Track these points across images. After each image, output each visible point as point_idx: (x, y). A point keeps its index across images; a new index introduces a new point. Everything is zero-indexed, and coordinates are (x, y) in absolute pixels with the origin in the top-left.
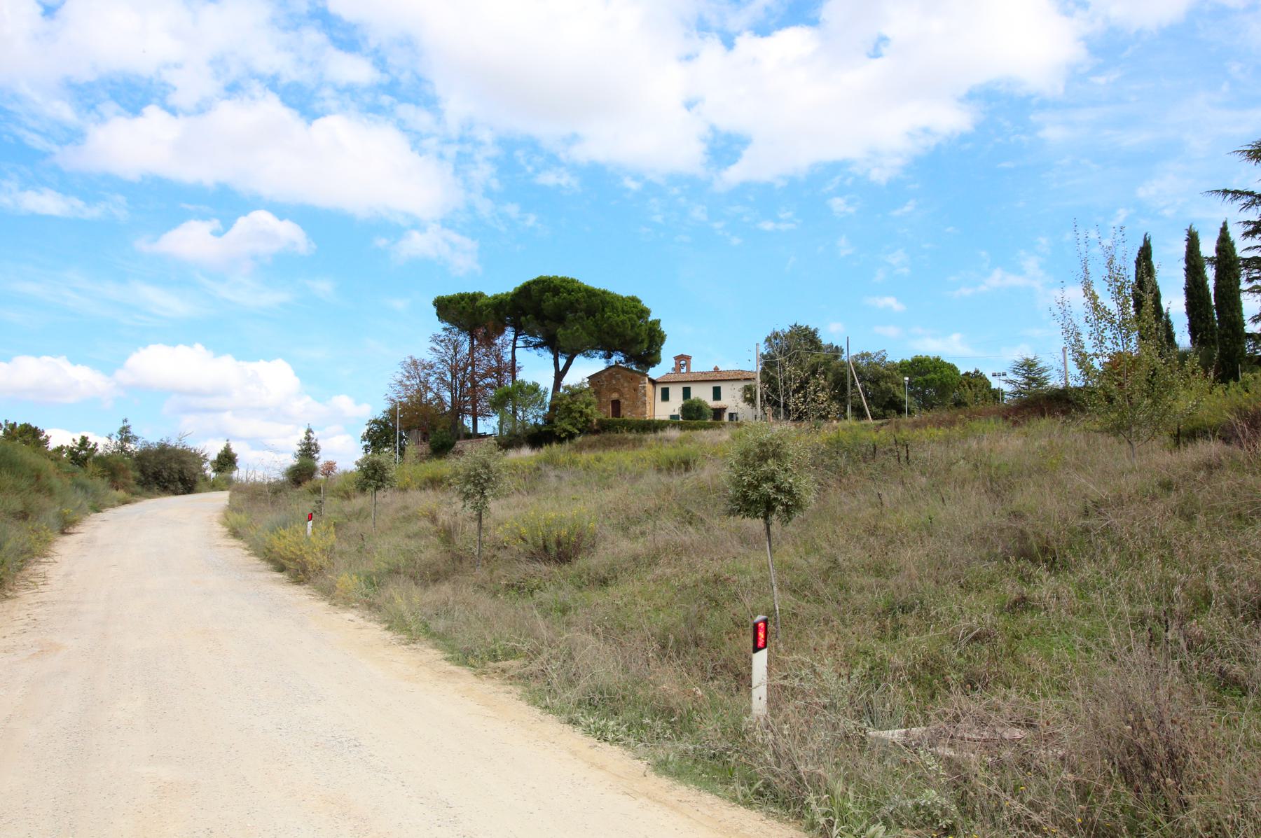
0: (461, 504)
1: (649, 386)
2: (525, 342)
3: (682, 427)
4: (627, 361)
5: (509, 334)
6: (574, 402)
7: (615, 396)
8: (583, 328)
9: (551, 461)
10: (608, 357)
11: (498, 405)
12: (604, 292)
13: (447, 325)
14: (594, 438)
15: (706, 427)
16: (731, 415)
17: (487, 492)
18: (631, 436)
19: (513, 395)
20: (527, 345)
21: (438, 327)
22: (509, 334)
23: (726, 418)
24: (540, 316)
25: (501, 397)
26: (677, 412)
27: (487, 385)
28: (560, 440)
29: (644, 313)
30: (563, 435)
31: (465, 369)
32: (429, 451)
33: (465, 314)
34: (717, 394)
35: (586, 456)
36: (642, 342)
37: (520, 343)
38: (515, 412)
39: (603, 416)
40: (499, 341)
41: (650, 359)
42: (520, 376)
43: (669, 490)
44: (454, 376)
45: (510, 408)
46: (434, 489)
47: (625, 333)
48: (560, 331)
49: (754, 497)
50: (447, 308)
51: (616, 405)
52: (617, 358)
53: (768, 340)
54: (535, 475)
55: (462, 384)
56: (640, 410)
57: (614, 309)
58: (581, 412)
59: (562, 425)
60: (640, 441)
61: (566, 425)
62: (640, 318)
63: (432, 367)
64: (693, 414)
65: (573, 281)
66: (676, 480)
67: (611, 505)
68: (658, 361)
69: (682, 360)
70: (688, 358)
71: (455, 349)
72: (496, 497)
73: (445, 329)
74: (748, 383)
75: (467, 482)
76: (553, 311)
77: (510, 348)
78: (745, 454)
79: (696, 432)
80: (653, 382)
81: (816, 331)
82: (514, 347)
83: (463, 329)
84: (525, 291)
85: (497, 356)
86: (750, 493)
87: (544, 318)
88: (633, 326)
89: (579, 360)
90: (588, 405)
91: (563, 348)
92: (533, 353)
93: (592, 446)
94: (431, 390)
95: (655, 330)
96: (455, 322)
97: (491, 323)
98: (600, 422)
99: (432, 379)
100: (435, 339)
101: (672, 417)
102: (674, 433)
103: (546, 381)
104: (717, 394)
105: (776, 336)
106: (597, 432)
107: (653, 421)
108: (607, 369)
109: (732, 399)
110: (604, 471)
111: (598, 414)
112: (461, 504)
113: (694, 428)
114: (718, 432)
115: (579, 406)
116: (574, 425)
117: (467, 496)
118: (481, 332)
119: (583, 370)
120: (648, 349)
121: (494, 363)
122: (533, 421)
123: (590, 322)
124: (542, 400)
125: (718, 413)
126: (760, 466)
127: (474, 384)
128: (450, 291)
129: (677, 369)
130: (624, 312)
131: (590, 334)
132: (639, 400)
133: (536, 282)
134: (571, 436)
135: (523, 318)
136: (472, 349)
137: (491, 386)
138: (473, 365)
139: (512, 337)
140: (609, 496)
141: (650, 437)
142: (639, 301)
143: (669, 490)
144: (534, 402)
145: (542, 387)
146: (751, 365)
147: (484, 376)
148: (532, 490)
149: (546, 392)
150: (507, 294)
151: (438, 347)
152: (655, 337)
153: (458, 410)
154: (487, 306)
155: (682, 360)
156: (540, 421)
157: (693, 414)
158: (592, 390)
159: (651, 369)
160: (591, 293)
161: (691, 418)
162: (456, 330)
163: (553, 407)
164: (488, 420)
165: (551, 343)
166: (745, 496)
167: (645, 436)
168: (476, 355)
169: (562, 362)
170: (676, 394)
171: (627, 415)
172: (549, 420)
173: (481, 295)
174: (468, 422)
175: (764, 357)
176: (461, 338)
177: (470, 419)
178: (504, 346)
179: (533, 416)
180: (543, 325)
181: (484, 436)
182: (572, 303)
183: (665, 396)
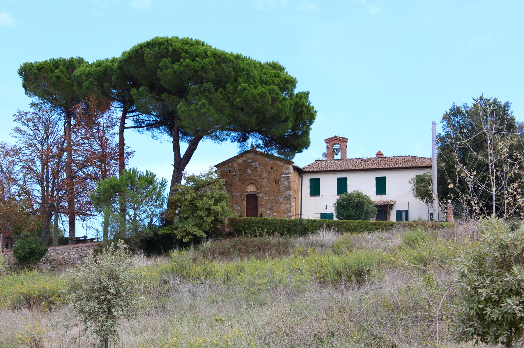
0: (82, 327)
1: (293, 176)
2: (137, 121)
3: (339, 228)
4: (266, 145)
5: (116, 111)
6: (201, 197)
7: (251, 189)
8: (211, 103)
9: (180, 272)
10: (243, 139)
11: (102, 201)
12: (238, 57)
13: (36, 99)
14: (226, 243)
15: (370, 229)
16: (399, 213)
17: (116, 312)
18: (273, 240)
19: (123, 188)
20: (139, 125)
21: (25, 102)
22: (116, 111)
23: (393, 217)
24: (156, 88)
25: (106, 190)
26: (331, 210)
27: (88, 176)
28: (183, 245)
29: (289, 83)
30: (185, 240)
31: (59, 156)
32: (13, 260)
33: (57, 84)
34: (381, 186)
35: (221, 266)
36: (286, 120)
37: (129, 122)
38: (123, 210)
39: (235, 215)
40: (103, 120)
41: (298, 142)
42: (130, 164)
43: (342, 310)
44: (45, 165)
45: (117, 206)
46: (31, 310)
47: (267, 109)
48: (181, 106)
49: (494, 316)
50: (38, 78)
51: (252, 200)
52: (254, 141)
53: (447, 117)
54: (163, 289)
55: (56, 175)
56: (283, 207)
57: (249, 77)
58: (209, 210)
59: (186, 227)
60: (286, 246)
61: (190, 226)
62: (283, 89)
63: (17, 154)
64: (353, 213)
65: (197, 43)
66: (351, 296)
67: (268, 328)
68: (306, 144)
69: (336, 143)
70: (343, 141)
71: (46, 130)
72: (127, 316)
73: (33, 105)
74: (421, 173)
75: (90, 299)
76: (173, 82)
77: (117, 129)
78: (480, 260)
79: (357, 235)
80: (300, 172)
81: (507, 105)
82: (123, 128)
83: (56, 104)
84: (137, 56)
85: (101, 138)
86: (488, 310)
87: (162, 90)
88: (274, 101)
89: (206, 144)
90: (217, 201)
91: (184, 129)
92: (146, 135)
93: (225, 254)
94: (15, 182)
95: (302, 105)
96: (45, 95)
97: (93, 98)
98: (232, 221)
99: (17, 168)
100: (21, 117)
101: (323, 216)
102: (328, 237)
103: (164, 172)
104: (381, 186)
105: (456, 112)
106: (229, 235)
107: (301, 221)
108: (241, 155)
109: (400, 191)
110: (252, 285)
111: (233, 211)
112: (82, 327)
113: (354, 230)
114: (386, 234)
115: (206, 202)
116: (199, 226)
117: (90, 316)
118: (80, 108)
119: (211, 155)
120: (293, 129)
121: (96, 147)
122: (147, 222)
123: (219, 95)
124: (159, 195)
125: (384, 210)
126: (499, 275)
127: (71, 175)
128: (40, 56)
129: (331, 153)
130: (264, 83)
131: (220, 110)
132: (281, 192)
133: (148, 45)
134: (197, 241)
135: (134, 91)
136: (69, 130)
137: (92, 177)
138: (69, 150)
139: (120, 114)
140: (267, 316)
141: (298, 242)
142: (282, 69)
143: (342, 310)
144: (148, 197)
145: (158, 179)
146: (426, 149)
147: (84, 165)
148: (161, 309)
149: (163, 185)
150: (113, 60)
151: (24, 128)
152: (303, 114)
153: (50, 208)
154: (88, 75)
155: (336, 143)
156: (156, 222)
157: (353, 213)
158: (222, 181)
159: (298, 156)
160: (220, 58)
161: (349, 218)
162: (48, 105)
163: (172, 204)
164: (89, 221)
165: (169, 122)
166: (481, 316)
167: (292, 240)
168: (73, 137)
169: (184, 146)
170: (329, 185)
171: (266, 212)
172: (167, 221)
173: (80, 61)
174: (63, 224)
175: (441, 139)
176: (54, 116)
177: (66, 219)
178: (110, 126)
179: (148, 216)
180: (160, 100)
181: (84, 240)
182: (196, 71)
183: (315, 190)
